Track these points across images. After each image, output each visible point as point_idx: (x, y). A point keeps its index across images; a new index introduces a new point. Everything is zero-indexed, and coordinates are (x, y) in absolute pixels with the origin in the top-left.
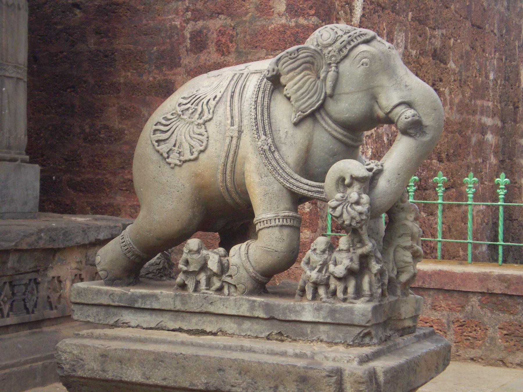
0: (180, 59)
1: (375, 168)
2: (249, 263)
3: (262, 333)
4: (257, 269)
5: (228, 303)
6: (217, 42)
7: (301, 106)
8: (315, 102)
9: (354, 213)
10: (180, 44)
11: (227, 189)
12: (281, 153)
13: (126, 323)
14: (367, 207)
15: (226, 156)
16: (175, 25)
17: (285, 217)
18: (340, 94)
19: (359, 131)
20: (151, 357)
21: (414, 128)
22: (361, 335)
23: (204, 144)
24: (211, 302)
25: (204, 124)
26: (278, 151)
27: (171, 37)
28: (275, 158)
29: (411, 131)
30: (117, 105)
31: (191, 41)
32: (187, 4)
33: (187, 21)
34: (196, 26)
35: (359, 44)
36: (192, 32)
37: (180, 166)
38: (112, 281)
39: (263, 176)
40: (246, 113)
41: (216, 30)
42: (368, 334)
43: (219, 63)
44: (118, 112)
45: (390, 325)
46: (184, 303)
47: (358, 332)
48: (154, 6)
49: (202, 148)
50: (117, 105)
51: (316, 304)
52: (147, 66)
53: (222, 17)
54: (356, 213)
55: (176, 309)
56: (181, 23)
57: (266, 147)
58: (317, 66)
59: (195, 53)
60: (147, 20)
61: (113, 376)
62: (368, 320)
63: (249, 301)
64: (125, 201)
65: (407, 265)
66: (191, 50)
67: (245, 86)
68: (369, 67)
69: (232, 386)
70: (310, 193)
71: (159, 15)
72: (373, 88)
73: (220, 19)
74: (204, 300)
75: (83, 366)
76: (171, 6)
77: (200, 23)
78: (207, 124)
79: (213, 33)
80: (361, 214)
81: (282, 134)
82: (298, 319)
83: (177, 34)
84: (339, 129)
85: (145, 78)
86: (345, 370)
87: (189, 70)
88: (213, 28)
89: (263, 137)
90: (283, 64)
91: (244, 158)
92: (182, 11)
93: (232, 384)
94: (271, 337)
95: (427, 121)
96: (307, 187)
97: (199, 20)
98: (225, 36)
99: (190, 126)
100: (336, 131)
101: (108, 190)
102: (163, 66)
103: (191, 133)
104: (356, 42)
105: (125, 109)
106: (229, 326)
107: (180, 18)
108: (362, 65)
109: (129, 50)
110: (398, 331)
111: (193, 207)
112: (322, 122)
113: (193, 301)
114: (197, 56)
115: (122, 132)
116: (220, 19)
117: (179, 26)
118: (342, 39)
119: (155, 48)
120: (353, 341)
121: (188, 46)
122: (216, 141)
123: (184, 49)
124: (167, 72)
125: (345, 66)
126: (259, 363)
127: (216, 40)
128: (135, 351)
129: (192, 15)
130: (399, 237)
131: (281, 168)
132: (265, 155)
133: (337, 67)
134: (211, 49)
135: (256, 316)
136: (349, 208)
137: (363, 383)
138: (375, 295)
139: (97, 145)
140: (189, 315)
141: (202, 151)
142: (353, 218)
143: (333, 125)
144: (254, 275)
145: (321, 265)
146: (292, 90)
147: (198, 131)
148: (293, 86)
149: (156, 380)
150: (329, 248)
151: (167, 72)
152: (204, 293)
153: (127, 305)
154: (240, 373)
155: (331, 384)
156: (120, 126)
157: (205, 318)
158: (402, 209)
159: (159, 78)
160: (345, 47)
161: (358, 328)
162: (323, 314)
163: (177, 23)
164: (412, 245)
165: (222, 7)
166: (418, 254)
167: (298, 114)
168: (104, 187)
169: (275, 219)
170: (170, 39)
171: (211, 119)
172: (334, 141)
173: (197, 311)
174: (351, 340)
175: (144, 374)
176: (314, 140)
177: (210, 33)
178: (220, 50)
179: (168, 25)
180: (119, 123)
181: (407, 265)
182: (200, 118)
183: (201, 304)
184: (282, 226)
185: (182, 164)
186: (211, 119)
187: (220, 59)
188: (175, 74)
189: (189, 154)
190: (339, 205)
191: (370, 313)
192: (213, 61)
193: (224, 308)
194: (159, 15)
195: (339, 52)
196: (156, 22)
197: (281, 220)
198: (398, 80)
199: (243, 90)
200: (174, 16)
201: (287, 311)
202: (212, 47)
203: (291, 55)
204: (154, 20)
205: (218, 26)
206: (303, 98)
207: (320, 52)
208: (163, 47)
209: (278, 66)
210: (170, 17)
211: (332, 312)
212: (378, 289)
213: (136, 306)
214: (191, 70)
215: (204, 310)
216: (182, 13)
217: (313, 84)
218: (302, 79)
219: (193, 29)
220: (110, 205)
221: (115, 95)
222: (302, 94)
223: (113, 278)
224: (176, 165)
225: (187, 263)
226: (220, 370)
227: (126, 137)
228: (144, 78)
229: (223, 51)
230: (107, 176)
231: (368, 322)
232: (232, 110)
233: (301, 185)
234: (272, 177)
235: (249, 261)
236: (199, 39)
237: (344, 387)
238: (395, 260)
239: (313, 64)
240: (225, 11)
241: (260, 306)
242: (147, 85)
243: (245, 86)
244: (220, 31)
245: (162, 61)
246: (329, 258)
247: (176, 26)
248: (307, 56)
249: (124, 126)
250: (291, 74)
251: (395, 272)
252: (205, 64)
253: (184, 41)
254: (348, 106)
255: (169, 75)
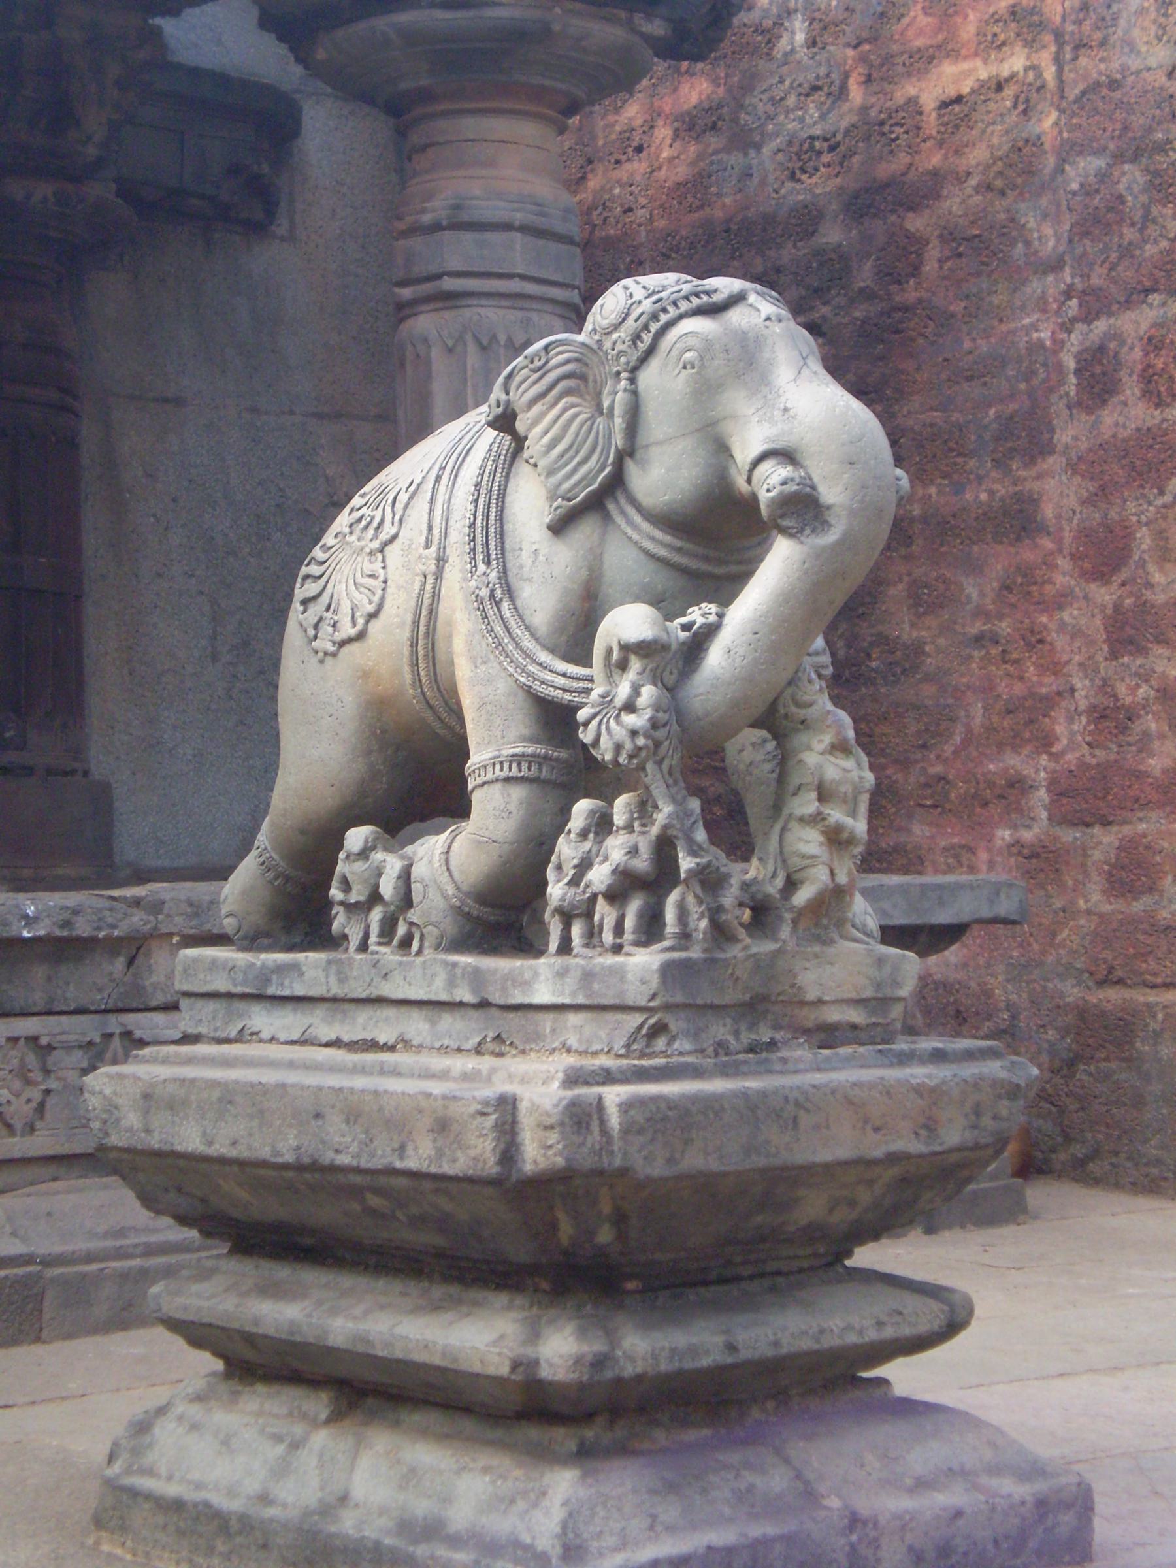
0: (1052, 431)
1: (700, 621)
2: (447, 874)
3: (468, 1039)
4: (465, 888)
5: (412, 974)
6: (1144, 370)
7: (560, 484)
8: (591, 473)
9: (619, 733)
10: (1051, 390)
11: (427, 702)
12: (519, 603)
13: (257, 1033)
14: (647, 716)
15: (414, 622)
16: (1039, 339)
17: (517, 759)
18: (647, 446)
19: (716, 535)
20: (216, 1094)
21: (802, 509)
22: (644, 1031)
23: (376, 599)
24: (384, 972)
25: (381, 551)
26: (512, 599)
27: (1029, 375)
28: (501, 617)
29: (785, 523)
30: (906, 579)
31: (1078, 379)
32: (1068, 280)
33: (1067, 327)
34: (1091, 335)
35: (680, 317)
36: (1080, 353)
37: (334, 655)
38: (252, 941)
39: (479, 660)
40: (456, 516)
41: (1141, 339)
42: (658, 1030)
43: (1148, 429)
44: (909, 597)
45: (770, 1017)
46: (342, 980)
47: (636, 1025)
48: (988, 299)
49: (371, 608)
50: (906, 579)
51: (559, 961)
52: (972, 463)
53: (1155, 298)
54: (624, 732)
55: (330, 995)
56: (1053, 333)
57: (484, 592)
58: (595, 382)
59: (1090, 410)
60: (974, 340)
61: (161, 1141)
62: (652, 992)
63: (446, 963)
64: (932, 837)
65: (808, 862)
66: (1079, 404)
67: (470, 449)
68: (698, 373)
69: (337, 1151)
70: (567, 696)
71: (1001, 321)
72: (714, 423)
73: (1151, 306)
74: (374, 971)
75: (118, 1120)
76: (1029, 290)
77: (1101, 326)
78: (388, 549)
79: (1132, 348)
80: (634, 733)
81: (526, 558)
82: (526, 1000)
83: (1045, 365)
84: (659, 534)
85: (969, 496)
86: (522, 1100)
87: (1075, 458)
88: (1133, 333)
89: (482, 567)
90: (518, 388)
91: (450, 623)
92: (1055, 300)
93: (336, 1146)
94: (484, 1048)
95: (831, 494)
96: (561, 681)
97: (1097, 318)
98: (1163, 352)
99: (359, 559)
100: (653, 539)
101: (894, 810)
102: (1012, 458)
103: (358, 575)
104: (673, 312)
105: (926, 587)
106: (416, 1026)
107: (1053, 319)
108: (685, 368)
109: (932, 425)
110: (806, 1032)
111: (369, 752)
112: (620, 520)
113: (355, 973)
114: (1094, 417)
115: (917, 649)
116: (1151, 306)
117: (1048, 343)
118: (639, 311)
119: (992, 412)
120: (627, 1046)
121: (1072, 393)
122: (399, 588)
123: (1062, 404)
124: (1023, 473)
125: (649, 377)
126: (376, 1093)
127: (1140, 367)
128: (193, 1081)
129: (1080, 305)
130: (794, 794)
131: (513, 639)
132: (484, 610)
133: (632, 380)
134: (1128, 392)
135: (458, 999)
136: (612, 723)
137: (552, 1127)
138: (694, 935)
139: (864, 690)
140: (352, 1006)
141: (373, 616)
142: (618, 748)
143: (646, 526)
144: (458, 904)
145: (575, 867)
146: (538, 447)
147: (368, 568)
148: (542, 437)
149: (221, 1146)
150: (598, 825)
151: (1023, 473)
152: (373, 953)
153: (254, 991)
154: (347, 1121)
155: (485, 1132)
156: (915, 634)
157: (378, 1012)
158: (803, 722)
159: (1003, 492)
160: (646, 327)
161: (637, 1015)
162: (571, 982)
163: (1045, 335)
164: (819, 813)
165: (1156, 271)
166: (845, 835)
167: (555, 504)
168: (884, 802)
169: (494, 764)
170: (1027, 381)
171: (394, 537)
172: (652, 566)
173: (364, 995)
174: (622, 1043)
175: (204, 1134)
176: (606, 566)
177: (1126, 349)
178: (1151, 393)
179: (1022, 345)
180: (912, 625)
181: (808, 862)
182: (375, 537)
183: (368, 980)
184: (507, 780)
185: (338, 650)
186: (394, 537)
187: (1152, 417)
188: (1039, 477)
189: (349, 624)
190: (594, 716)
191: (656, 976)
192: (1133, 426)
193: (407, 986)
194: (1001, 321)
195: (634, 343)
196: (993, 340)
197: (506, 766)
198: (769, 396)
199: (463, 460)
200: (1036, 316)
201: (509, 983)
202: (1131, 388)
203: (532, 362)
204: (988, 337)
205: (1144, 326)
206: (566, 465)
207: (595, 347)
208: (1011, 406)
209: (507, 393)
210: (1027, 321)
211: (588, 976)
212: (699, 919)
213: (271, 991)
214: (1080, 458)
215: (375, 992)
216: (1055, 306)
217: (585, 428)
218: (559, 417)
219: (1081, 344)
220: (898, 849)
221: (903, 551)
222: (562, 456)
223: (252, 933)
224: (326, 654)
225: (346, 886)
226: (318, 1116)
227: (929, 660)
228: (967, 496)
229: (1159, 394)
230: (888, 772)
231: (653, 997)
232: (431, 510)
233: (549, 677)
234: (495, 664)
235: (448, 869)
236: (1098, 369)
237: (519, 1139)
238: (781, 852)
239: (583, 377)
240: (1163, 281)
241: (463, 975)
242: (973, 515)
243: (470, 449)
244: (1150, 339)
245: (1009, 445)
246: (594, 850)
247: (1040, 344)
248: (568, 362)
249: (923, 633)
250: (537, 409)
251: (779, 882)
252: (1114, 436)
253: (1062, 382)
254: (666, 474)
255: (1025, 479)
